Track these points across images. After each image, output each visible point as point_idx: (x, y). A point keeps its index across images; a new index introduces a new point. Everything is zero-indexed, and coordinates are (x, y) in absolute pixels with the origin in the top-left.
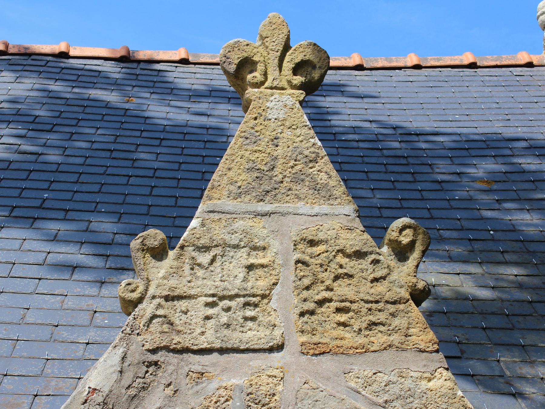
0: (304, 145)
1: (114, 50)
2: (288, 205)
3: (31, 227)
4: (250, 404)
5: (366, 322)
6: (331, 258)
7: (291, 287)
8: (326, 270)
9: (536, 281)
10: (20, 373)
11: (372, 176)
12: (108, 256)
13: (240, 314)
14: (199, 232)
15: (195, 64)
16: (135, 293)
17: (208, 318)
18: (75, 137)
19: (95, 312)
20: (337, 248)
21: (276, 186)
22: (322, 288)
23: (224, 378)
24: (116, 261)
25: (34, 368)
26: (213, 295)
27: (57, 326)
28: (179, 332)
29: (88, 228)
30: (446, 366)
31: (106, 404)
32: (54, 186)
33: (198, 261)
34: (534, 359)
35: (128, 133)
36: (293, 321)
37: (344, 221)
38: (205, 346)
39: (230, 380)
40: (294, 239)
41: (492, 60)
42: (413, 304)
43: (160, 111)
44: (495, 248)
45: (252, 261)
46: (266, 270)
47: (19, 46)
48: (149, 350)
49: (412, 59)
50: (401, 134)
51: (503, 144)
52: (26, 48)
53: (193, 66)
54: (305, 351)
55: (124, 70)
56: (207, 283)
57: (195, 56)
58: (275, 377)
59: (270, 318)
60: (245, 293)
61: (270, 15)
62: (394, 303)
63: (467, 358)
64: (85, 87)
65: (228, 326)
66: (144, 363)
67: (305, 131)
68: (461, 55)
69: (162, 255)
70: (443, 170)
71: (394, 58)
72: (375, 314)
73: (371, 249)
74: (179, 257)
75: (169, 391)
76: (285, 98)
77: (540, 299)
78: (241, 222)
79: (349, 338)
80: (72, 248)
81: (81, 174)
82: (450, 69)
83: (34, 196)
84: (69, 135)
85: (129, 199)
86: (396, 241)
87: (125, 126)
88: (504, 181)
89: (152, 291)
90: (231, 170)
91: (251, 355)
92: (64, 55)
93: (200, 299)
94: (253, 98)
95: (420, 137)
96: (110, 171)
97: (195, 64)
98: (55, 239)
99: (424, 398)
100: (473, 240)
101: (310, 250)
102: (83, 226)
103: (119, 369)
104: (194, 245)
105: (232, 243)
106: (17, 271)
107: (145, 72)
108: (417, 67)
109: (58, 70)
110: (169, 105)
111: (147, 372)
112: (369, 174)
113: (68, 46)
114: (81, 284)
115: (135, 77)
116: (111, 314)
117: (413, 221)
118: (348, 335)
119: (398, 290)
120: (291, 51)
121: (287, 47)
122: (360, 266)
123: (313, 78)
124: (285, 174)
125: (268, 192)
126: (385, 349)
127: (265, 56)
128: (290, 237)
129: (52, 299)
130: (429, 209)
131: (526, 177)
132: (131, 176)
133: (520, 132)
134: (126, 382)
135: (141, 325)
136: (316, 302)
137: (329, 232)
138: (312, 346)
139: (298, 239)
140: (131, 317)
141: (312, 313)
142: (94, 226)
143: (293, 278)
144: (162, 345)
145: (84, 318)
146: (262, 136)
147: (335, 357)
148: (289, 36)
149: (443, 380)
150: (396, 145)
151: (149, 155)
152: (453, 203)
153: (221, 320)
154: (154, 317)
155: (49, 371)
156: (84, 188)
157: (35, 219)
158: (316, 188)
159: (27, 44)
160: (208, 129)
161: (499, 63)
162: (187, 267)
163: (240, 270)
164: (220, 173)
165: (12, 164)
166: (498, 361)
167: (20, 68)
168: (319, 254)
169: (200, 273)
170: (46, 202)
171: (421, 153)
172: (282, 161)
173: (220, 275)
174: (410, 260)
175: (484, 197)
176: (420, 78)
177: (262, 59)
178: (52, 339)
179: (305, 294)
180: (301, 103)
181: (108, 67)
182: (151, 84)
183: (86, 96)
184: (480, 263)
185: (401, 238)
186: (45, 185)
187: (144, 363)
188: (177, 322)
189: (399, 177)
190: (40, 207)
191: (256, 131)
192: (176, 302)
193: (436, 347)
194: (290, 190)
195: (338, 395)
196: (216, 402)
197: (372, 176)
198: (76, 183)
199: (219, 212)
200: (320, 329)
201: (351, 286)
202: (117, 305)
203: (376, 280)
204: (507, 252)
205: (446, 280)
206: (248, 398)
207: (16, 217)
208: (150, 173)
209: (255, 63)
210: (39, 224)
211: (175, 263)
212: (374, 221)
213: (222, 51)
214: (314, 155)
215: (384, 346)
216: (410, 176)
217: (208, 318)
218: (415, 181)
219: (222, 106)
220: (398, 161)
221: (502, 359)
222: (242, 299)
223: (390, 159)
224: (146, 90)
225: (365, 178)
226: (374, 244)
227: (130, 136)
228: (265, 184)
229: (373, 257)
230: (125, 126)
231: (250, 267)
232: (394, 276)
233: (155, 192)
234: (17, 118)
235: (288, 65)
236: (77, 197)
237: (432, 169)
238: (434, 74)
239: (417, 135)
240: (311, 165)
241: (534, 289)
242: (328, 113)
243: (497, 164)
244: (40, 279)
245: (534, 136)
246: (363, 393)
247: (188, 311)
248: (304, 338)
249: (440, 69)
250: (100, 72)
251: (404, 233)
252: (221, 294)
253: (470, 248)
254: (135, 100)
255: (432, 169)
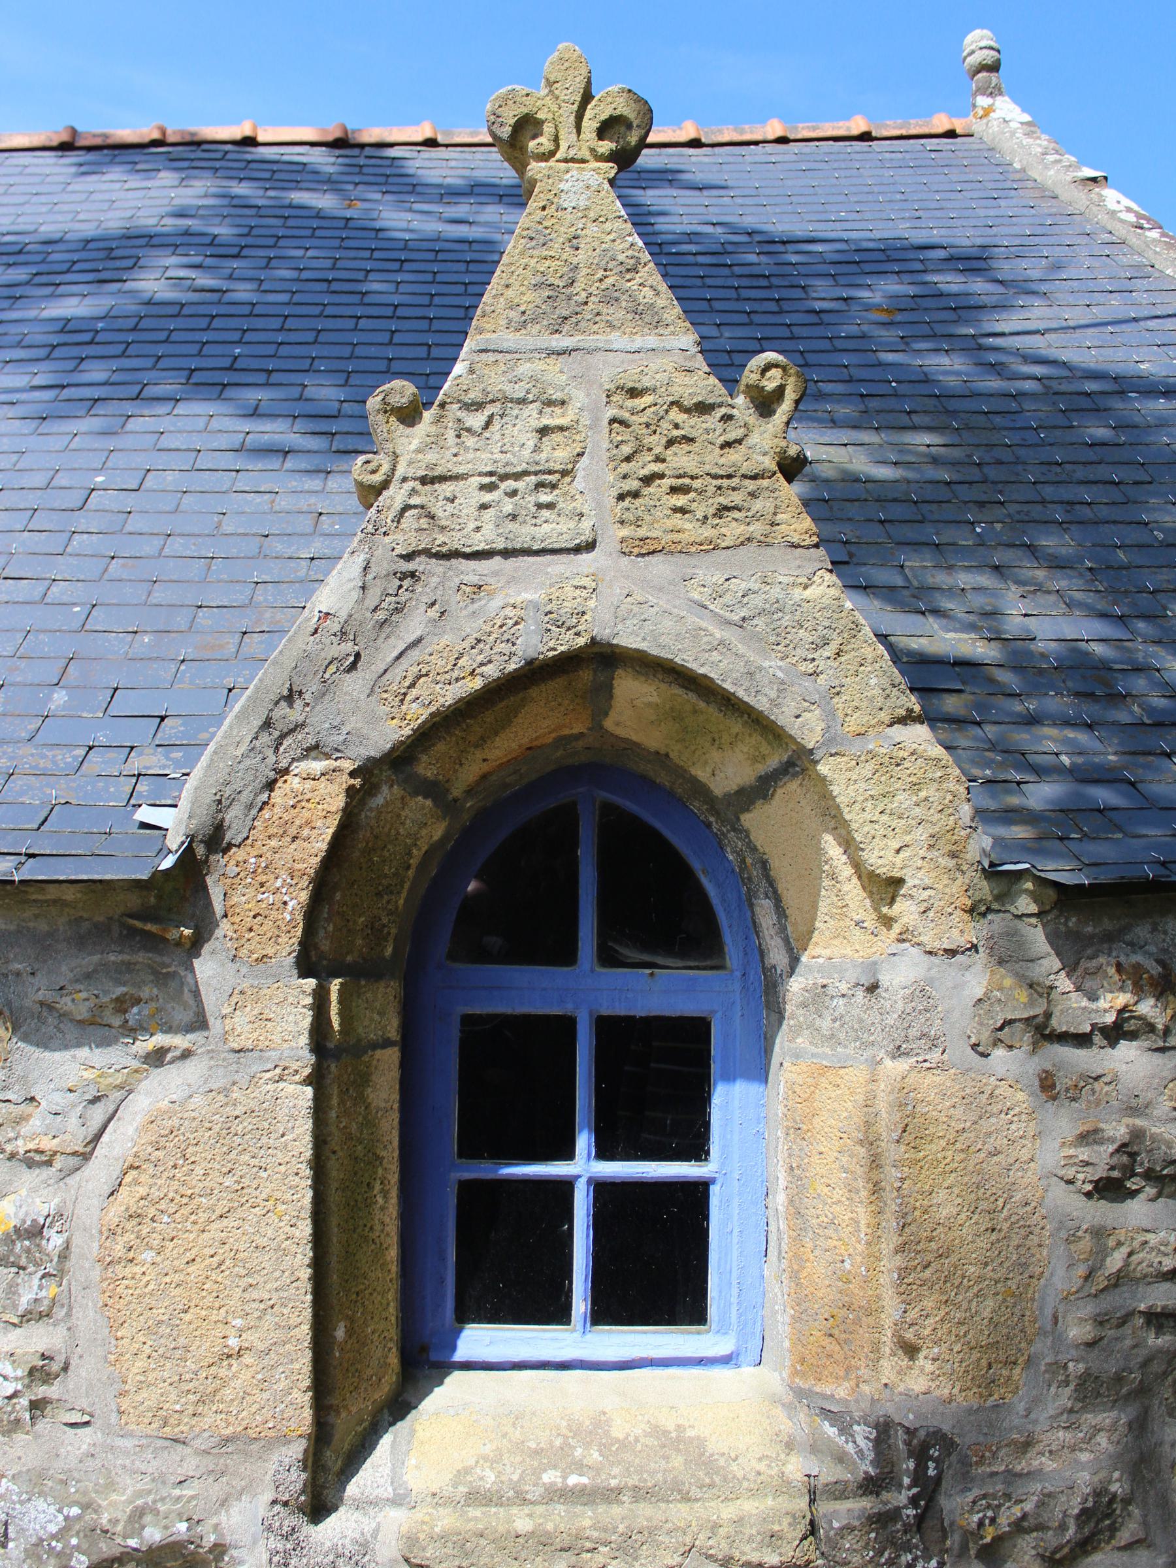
0: (619, 246)
1: (324, 131)
2: (596, 337)
3: (219, 397)
4: (550, 627)
5: (715, 506)
6: (662, 413)
7: (605, 458)
8: (655, 432)
9: (957, 453)
10: (220, 604)
11: (717, 305)
12: (333, 434)
13: (531, 499)
14: (466, 382)
15: (447, 146)
16: (378, 474)
17: (484, 507)
18: (274, 263)
19: (321, 514)
20: (671, 399)
21: (578, 309)
22: (650, 458)
23: (511, 592)
24: (345, 435)
25: (240, 595)
26: (491, 474)
27: (267, 536)
28: (443, 528)
29: (301, 395)
30: (830, 567)
31: (345, 633)
32: (248, 337)
33: (467, 425)
34: (953, 562)
35: (352, 254)
36: (609, 506)
37: (679, 358)
38: (482, 547)
39: (519, 595)
40: (607, 387)
41: (894, 128)
42: (782, 479)
43: (399, 219)
44: (898, 407)
45: (546, 421)
46: (566, 434)
47: (182, 132)
48: (401, 556)
49: (775, 129)
50: (759, 242)
51: (911, 255)
52: (193, 134)
53: (444, 149)
54: (627, 550)
55: (340, 160)
56: (481, 457)
57: (447, 133)
58: (585, 588)
59: (574, 504)
60: (538, 468)
61: (560, 46)
62: (754, 477)
63: (857, 564)
64: (283, 189)
65: (514, 517)
66: (395, 574)
67: (619, 224)
68: (848, 119)
69: (414, 418)
70: (823, 294)
71: (747, 127)
72: (729, 491)
73: (719, 400)
74: (438, 420)
75: (433, 613)
76: (586, 175)
77: (962, 479)
78: (528, 365)
79: (690, 529)
80: (281, 425)
81: (286, 317)
82: (831, 143)
83: (220, 353)
84: (266, 260)
85: (359, 351)
86: (757, 386)
87: (346, 243)
88: (912, 310)
89: (400, 471)
90: (507, 292)
91: (549, 558)
92: (249, 142)
93: (472, 479)
94: (538, 177)
95: (788, 245)
96: (329, 311)
97: (447, 146)
98: (255, 413)
99: (798, 613)
100: (867, 395)
101: (630, 403)
102: (295, 392)
103: (360, 584)
104: (459, 401)
105: (515, 396)
106: (204, 461)
107: (373, 162)
108: (783, 140)
109: (242, 165)
110: (411, 210)
111: (400, 587)
112: (714, 303)
113: (255, 128)
114: (297, 475)
115: (357, 170)
116: (343, 516)
117: (780, 358)
118: (688, 526)
119: (761, 458)
120: (593, 103)
121: (587, 97)
122: (704, 426)
123: (629, 143)
124: (590, 291)
125: (566, 318)
126: (742, 544)
127: (555, 111)
128: (601, 385)
129: (258, 499)
130: (802, 353)
131: (943, 302)
132: (360, 317)
133: (935, 235)
134: (371, 602)
135: (389, 521)
136: (641, 479)
137: (657, 376)
138: (637, 543)
139: (612, 387)
140: (373, 510)
141: (636, 495)
142: (310, 392)
143: (606, 445)
144: (420, 548)
145: (306, 523)
146: (554, 235)
147: (669, 557)
148: (589, 78)
149: (825, 587)
150: (753, 258)
151: (385, 285)
152: (837, 343)
153: (504, 510)
154: (407, 508)
155: (261, 598)
156: (293, 337)
157: (225, 385)
158: (637, 312)
159: (193, 128)
160: (470, 243)
161: (904, 132)
162: (450, 435)
163: (529, 435)
164: (494, 292)
165: (185, 308)
166: (902, 567)
167: (185, 164)
168: (644, 409)
169: (471, 441)
170: (239, 360)
171: (788, 270)
172: (584, 271)
173: (500, 444)
174: (777, 415)
175: (883, 332)
176: (787, 158)
177: (550, 116)
178: (261, 555)
179: (625, 468)
180: (612, 182)
181: (319, 158)
182: (382, 180)
183: (287, 202)
184: (876, 429)
185: (764, 383)
186: (236, 336)
187: (395, 574)
188: (440, 514)
189: (757, 306)
190: (230, 368)
191: (546, 228)
192: (437, 486)
193: (815, 539)
194: (598, 314)
195: (675, 611)
196: (501, 627)
197: (717, 305)
198: (280, 330)
199: (494, 351)
200: (647, 517)
201: (692, 455)
202: (354, 502)
203: (727, 445)
204: (915, 412)
205: (827, 453)
206: (546, 619)
207: (197, 384)
208: (389, 311)
209: (539, 123)
210: (230, 392)
211: (433, 429)
212: (725, 364)
213: (489, 107)
214: (632, 262)
215: (741, 540)
216: (774, 304)
217: (484, 507)
218: (780, 312)
219: (490, 209)
220: (755, 283)
221: (907, 564)
222: (533, 477)
223: (744, 279)
224: (376, 188)
225: (708, 309)
226: (724, 391)
227: (355, 259)
228: (561, 306)
229: (723, 410)
230: (346, 243)
231: (544, 431)
232: (754, 439)
233: (397, 338)
234: (187, 239)
235: (590, 125)
236: (284, 351)
237: (806, 292)
238: (807, 150)
239: (784, 243)
240: (628, 277)
241: (953, 464)
242: (650, 214)
243: (902, 283)
244: (238, 471)
245: (957, 242)
246: (711, 607)
247: (455, 497)
248: (625, 532)
249: (817, 143)
250: (305, 164)
251: (768, 374)
252: (502, 471)
253: (862, 407)
254: (359, 205)
255: (806, 292)
